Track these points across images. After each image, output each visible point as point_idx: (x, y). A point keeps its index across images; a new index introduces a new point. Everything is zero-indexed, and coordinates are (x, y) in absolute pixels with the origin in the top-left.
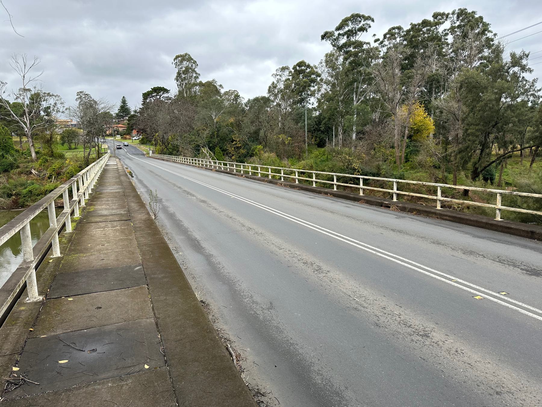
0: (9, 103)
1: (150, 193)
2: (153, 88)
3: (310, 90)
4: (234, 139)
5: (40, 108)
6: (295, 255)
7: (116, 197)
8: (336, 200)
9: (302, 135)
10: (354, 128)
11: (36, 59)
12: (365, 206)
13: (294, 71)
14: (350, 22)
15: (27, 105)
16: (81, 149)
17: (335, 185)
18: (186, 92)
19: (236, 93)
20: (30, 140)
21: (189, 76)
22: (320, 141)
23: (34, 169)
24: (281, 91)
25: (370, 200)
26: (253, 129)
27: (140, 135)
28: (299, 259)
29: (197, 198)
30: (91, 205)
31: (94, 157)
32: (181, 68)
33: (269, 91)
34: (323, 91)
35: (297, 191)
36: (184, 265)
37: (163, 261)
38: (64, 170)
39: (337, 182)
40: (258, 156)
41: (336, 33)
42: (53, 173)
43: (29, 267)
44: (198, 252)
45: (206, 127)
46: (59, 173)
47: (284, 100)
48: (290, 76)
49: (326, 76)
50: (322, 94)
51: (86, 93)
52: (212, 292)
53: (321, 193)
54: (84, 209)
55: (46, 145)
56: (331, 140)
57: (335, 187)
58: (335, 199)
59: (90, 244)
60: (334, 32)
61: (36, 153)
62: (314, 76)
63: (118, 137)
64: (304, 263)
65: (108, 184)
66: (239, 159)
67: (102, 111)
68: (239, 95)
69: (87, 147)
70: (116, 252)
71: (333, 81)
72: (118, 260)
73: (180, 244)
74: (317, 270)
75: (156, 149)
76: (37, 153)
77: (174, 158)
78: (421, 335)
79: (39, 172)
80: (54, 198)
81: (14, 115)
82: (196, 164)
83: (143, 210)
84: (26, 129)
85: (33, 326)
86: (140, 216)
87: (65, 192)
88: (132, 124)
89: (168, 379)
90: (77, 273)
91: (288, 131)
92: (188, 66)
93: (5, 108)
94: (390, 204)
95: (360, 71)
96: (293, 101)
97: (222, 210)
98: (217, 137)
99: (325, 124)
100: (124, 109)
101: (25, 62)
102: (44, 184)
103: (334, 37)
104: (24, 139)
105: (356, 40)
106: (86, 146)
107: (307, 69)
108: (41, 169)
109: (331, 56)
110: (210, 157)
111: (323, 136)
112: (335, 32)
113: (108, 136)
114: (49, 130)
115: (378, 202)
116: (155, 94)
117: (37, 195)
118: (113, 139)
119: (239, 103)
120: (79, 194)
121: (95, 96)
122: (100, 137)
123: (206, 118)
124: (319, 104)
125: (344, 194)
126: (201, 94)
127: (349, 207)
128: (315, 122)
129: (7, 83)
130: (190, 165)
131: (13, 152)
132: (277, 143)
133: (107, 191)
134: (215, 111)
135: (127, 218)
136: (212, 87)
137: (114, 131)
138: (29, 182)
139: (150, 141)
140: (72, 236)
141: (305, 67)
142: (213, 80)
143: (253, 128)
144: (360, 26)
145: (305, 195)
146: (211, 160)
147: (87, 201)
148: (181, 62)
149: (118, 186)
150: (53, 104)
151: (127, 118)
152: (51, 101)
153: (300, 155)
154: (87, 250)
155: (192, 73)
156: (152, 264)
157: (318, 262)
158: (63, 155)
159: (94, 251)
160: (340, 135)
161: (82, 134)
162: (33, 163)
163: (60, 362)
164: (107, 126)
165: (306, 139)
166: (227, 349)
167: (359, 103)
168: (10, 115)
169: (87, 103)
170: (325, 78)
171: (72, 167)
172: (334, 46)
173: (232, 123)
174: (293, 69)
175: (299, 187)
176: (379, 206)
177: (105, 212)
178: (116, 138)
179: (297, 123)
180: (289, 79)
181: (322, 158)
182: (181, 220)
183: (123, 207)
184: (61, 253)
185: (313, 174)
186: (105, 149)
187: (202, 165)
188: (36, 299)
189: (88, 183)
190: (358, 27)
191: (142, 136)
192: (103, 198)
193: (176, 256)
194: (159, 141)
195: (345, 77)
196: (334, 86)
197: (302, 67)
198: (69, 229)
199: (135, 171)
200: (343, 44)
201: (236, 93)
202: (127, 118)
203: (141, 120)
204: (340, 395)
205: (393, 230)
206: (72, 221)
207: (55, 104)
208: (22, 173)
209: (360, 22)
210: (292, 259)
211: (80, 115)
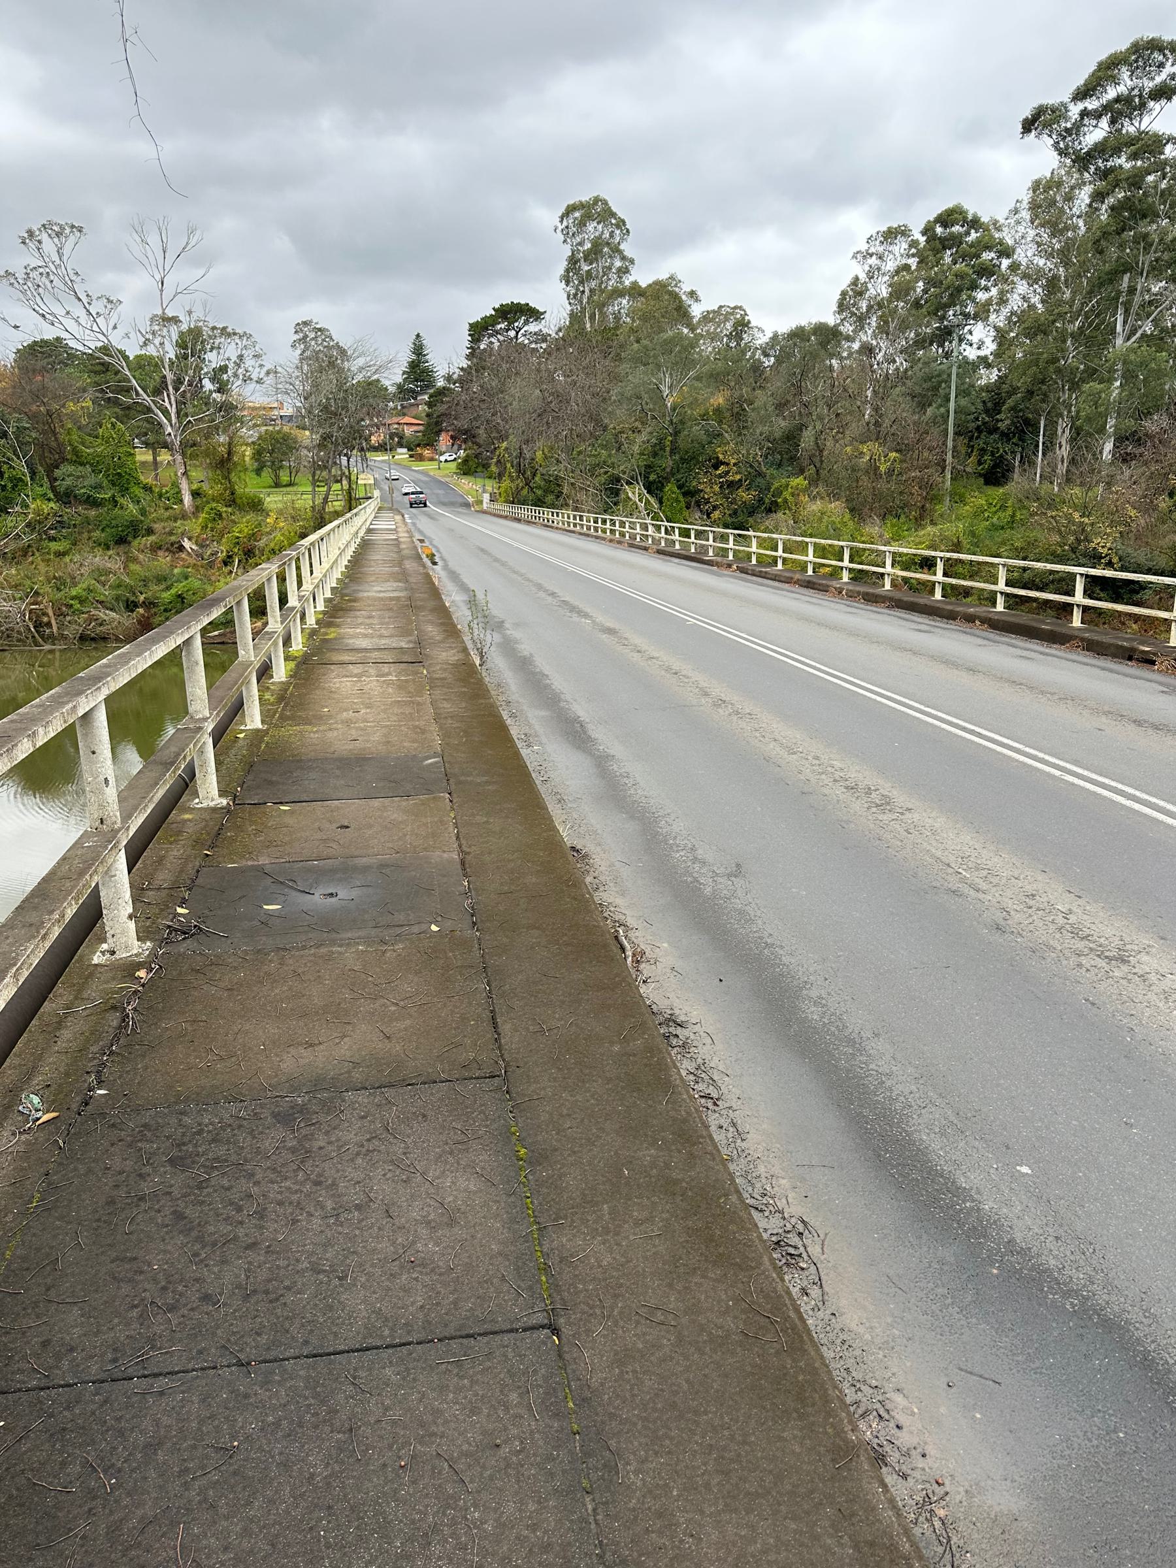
0: (126, 358)
1: (472, 602)
2: (497, 306)
3: (974, 300)
4: (721, 457)
5: (202, 369)
6: (829, 769)
7: (391, 609)
8: (997, 638)
9: (934, 444)
10: (1111, 422)
11: (191, 231)
12: (1080, 658)
13: (927, 241)
14: (1124, 69)
15: (171, 362)
16: (305, 485)
17: (1002, 593)
18: (592, 317)
19: (738, 316)
20: (179, 458)
21: (603, 268)
22: (995, 466)
23: (190, 539)
24: (880, 305)
25: (1098, 642)
26: (781, 425)
27: (460, 448)
28: (838, 778)
29: (594, 622)
30: (330, 625)
31: (339, 509)
32: (581, 244)
33: (842, 306)
34: (1015, 302)
35: (883, 610)
36: (542, 772)
37: (490, 752)
38: (261, 543)
39: (1007, 585)
40: (790, 509)
41: (1075, 110)
42: (236, 550)
43: (200, 728)
44: (579, 748)
45: (643, 423)
46: (249, 551)
47: (887, 334)
48: (913, 255)
49: (1029, 254)
50: (1013, 313)
51: (318, 326)
52: (599, 831)
53: (954, 619)
54: (313, 633)
55: (218, 472)
56: (1028, 462)
57: (1000, 600)
58: (993, 635)
59: (327, 707)
60: (1066, 108)
61: (193, 495)
62: (993, 255)
63: (402, 454)
64: (847, 788)
65: (373, 578)
66: (733, 520)
67: (359, 377)
68: (749, 322)
69: (320, 481)
70: (387, 726)
71: (1050, 270)
72: (388, 742)
73: (537, 727)
74: (877, 806)
75: (502, 490)
76: (196, 494)
77: (546, 513)
78: (1107, 957)
79: (202, 546)
80: (247, 589)
81: (139, 389)
82: (604, 531)
83: (453, 642)
84: (169, 430)
85: (210, 848)
86: (446, 656)
87: (269, 580)
88: (439, 417)
89: (474, 949)
90: (298, 761)
91: (892, 431)
92: (600, 237)
93: (117, 372)
94: (1155, 654)
95: (1146, 236)
96: (917, 335)
97: (656, 654)
98: (672, 452)
99: (1013, 409)
100: (418, 371)
101: (165, 240)
102: (213, 578)
103: (1066, 122)
104: (164, 457)
105: (1142, 128)
106: (316, 477)
107: (968, 233)
108: (207, 539)
109: (1050, 188)
110: (648, 515)
111: (1004, 448)
112: (1071, 106)
113: (375, 449)
114: (224, 431)
115: (1122, 646)
116: (503, 326)
118: (387, 458)
119: (748, 347)
120: (303, 594)
121: (342, 336)
122: (355, 452)
123: (643, 393)
124: (1000, 345)
125: (1022, 622)
126: (634, 321)
127: (1029, 658)
128: (984, 402)
129: (121, 302)
130: (588, 535)
131: (137, 491)
132: (854, 470)
133: (370, 594)
134: (671, 374)
135: (414, 658)
136: (666, 297)
137: (392, 436)
138: (176, 571)
139: (486, 466)
140: (286, 690)
141: (963, 226)
142: (672, 278)
143: (783, 424)
144: (1158, 79)
145: (904, 623)
146: (648, 521)
147: (321, 616)
148: (582, 224)
149: (397, 584)
150: (234, 358)
151: (426, 397)
152: (231, 351)
153: (923, 507)
154: (320, 719)
155: (610, 257)
156: (463, 755)
157: (886, 787)
158: (260, 501)
159: (336, 723)
160: (1060, 447)
161: (307, 442)
162: (186, 523)
163: (265, 907)
164: (371, 420)
165: (949, 458)
166: (616, 938)
167: (1133, 339)
168: (128, 390)
169: (321, 355)
170: (1024, 262)
171: (283, 535)
172: (1062, 153)
173: (718, 411)
174: (924, 233)
175: (891, 599)
176: (1123, 658)
177: (364, 643)
178: (396, 457)
179: (923, 406)
180: (906, 267)
181: (995, 520)
182: (546, 673)
183: (404, 632)
184: (263, 722)
185: (939, 560)
186: (368, 488)
187: (622, 535)
188: (214, 803)
189: (324, 571)
190: (1151, 84)
191: (465, 450)
192: (359, 610)
193: (524, 752)
194: (509, 465)
195: (1093, 255)
196: (1052, 285)
197: (952, 225)
198: (281, 672)
199: (442, 549)
200: (1096, 144)
201: (738, 316)
202: (426, 397)
203: (462, 403)
204: (857, 1046)
205: (1138, 723)
206: (287, 658)
207: (241, 357)
208: (160, 548)
209: (1159, 67)
210: (818, 777)
211: (304, 390)
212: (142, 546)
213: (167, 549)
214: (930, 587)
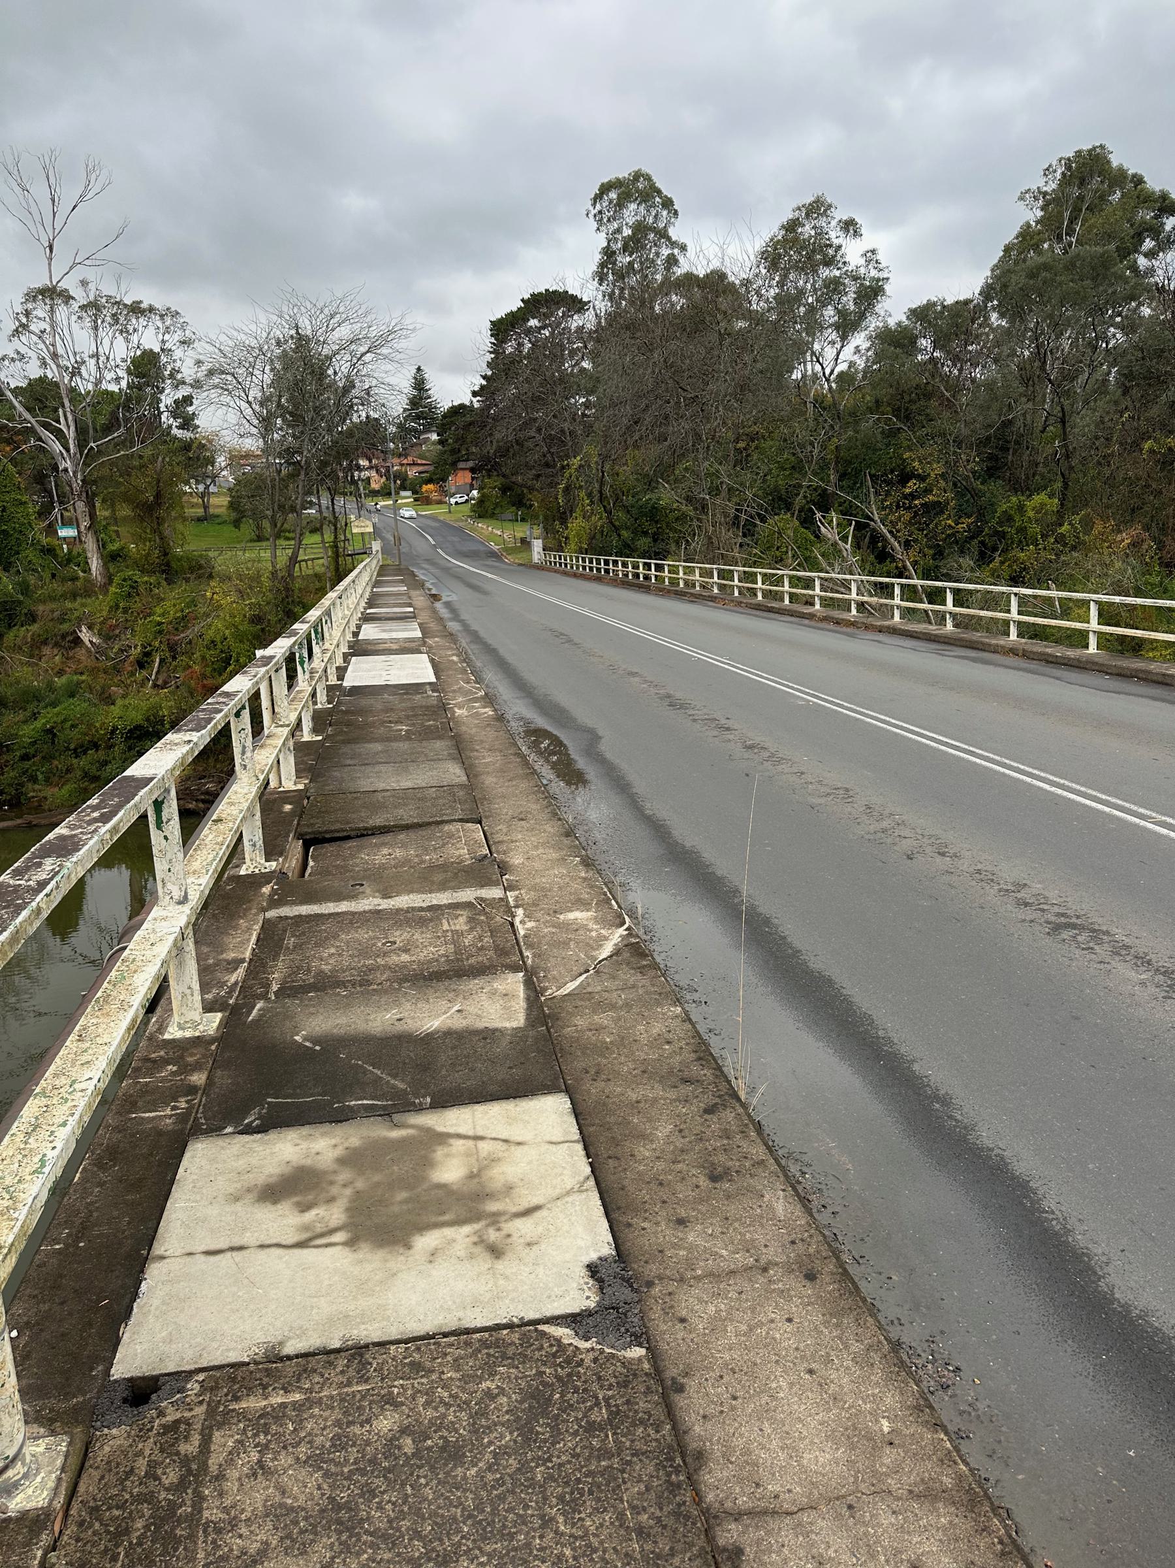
2: (527, 296)
23: (90, 628)
108: (117, 626)
117: (75, 750)
148: (620, 205)
162: (89, 601)
208: (45, 642)
212: (18, 641)
213: (56, 645)
214: (1080, 639)
